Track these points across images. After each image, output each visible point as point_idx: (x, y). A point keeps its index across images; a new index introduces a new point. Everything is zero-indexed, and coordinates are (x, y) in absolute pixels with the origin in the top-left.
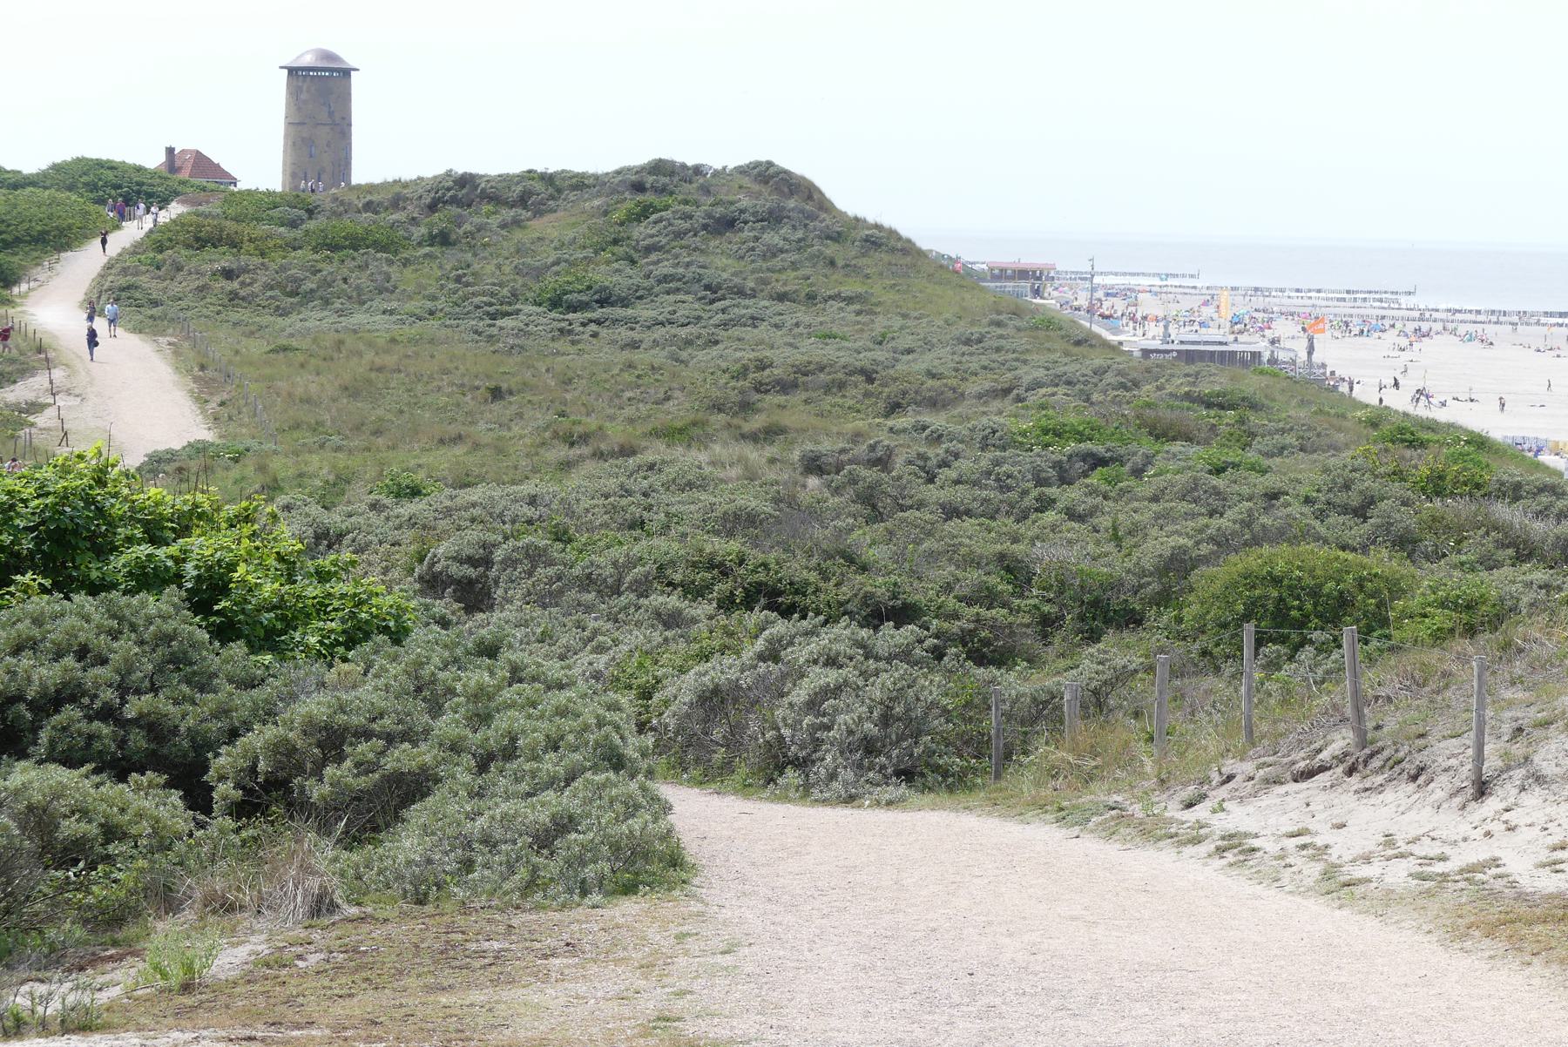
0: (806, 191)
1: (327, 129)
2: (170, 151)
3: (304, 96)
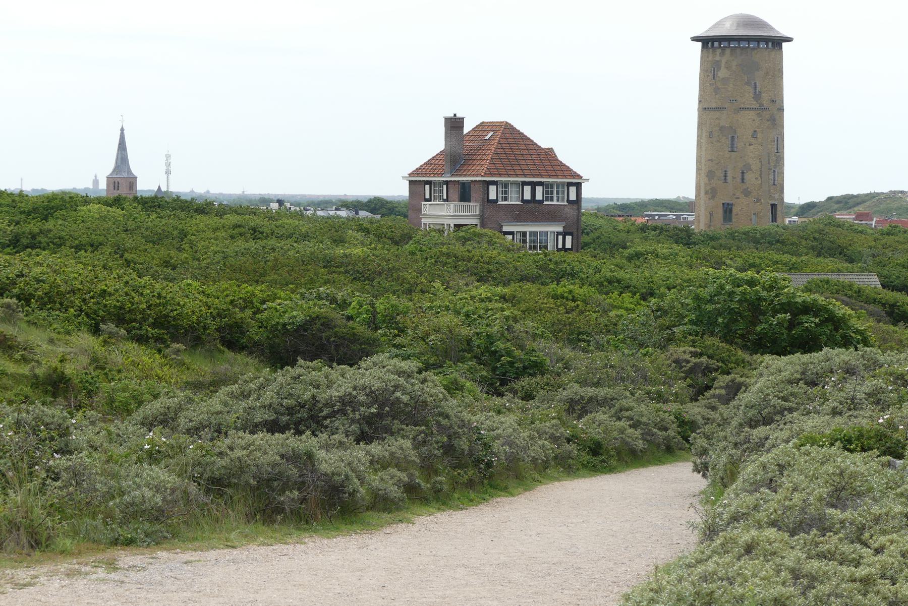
0: (544, 161)
1: (752, 114)
2: (454, 124)
3: (723, 73)
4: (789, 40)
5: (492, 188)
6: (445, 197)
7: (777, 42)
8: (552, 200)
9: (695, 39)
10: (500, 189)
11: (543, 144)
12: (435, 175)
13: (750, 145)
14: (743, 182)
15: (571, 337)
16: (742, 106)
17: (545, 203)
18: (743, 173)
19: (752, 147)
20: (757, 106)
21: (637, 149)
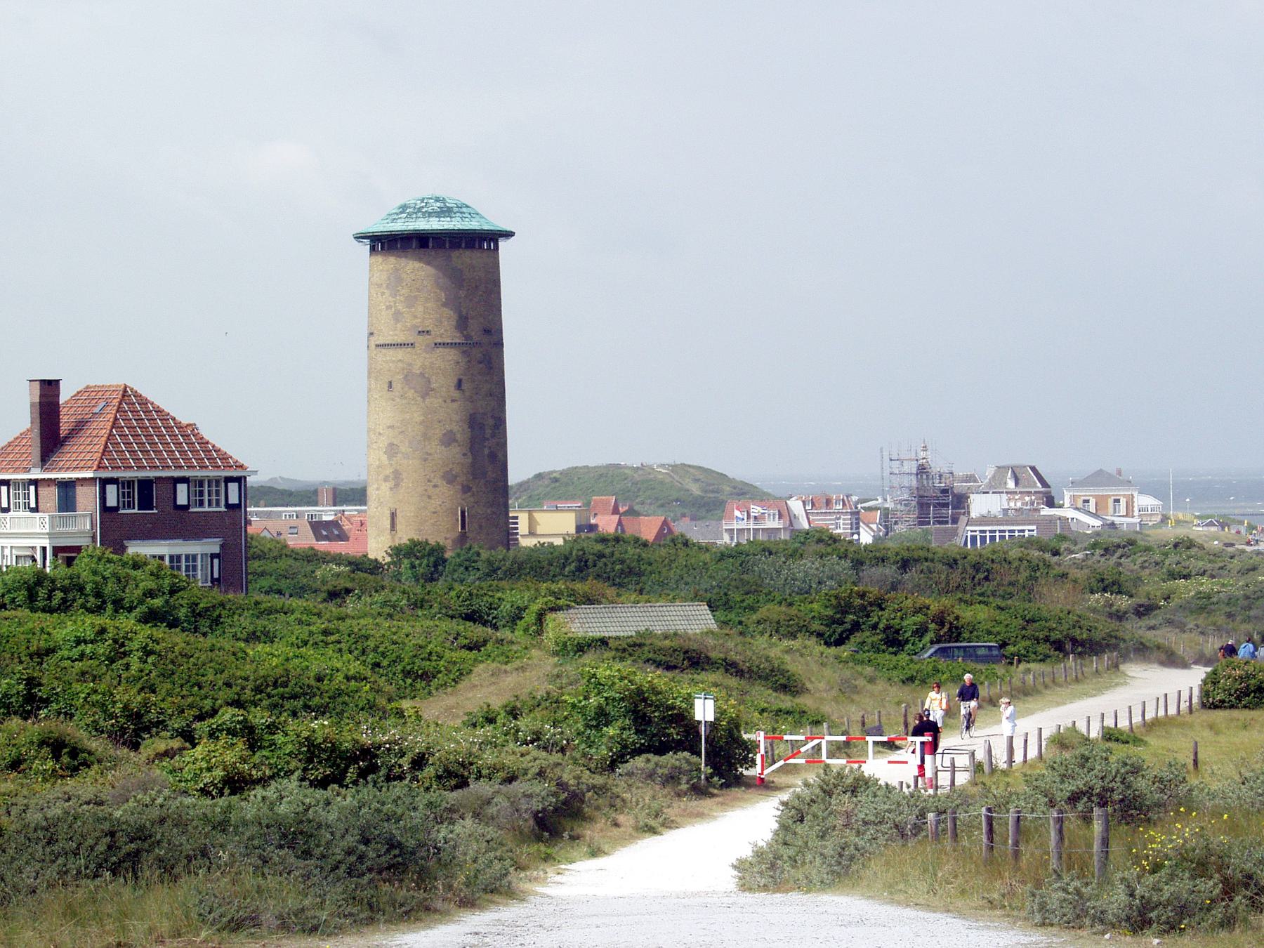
4: (508, 235)
5: (182, 489)
6: (33, 505)
8: (201, 504)
9: (360, 237)
10: (192, 489)
11: (183, 417)
12: (16, 470)
17: (121, 511)
21: (313, 419)
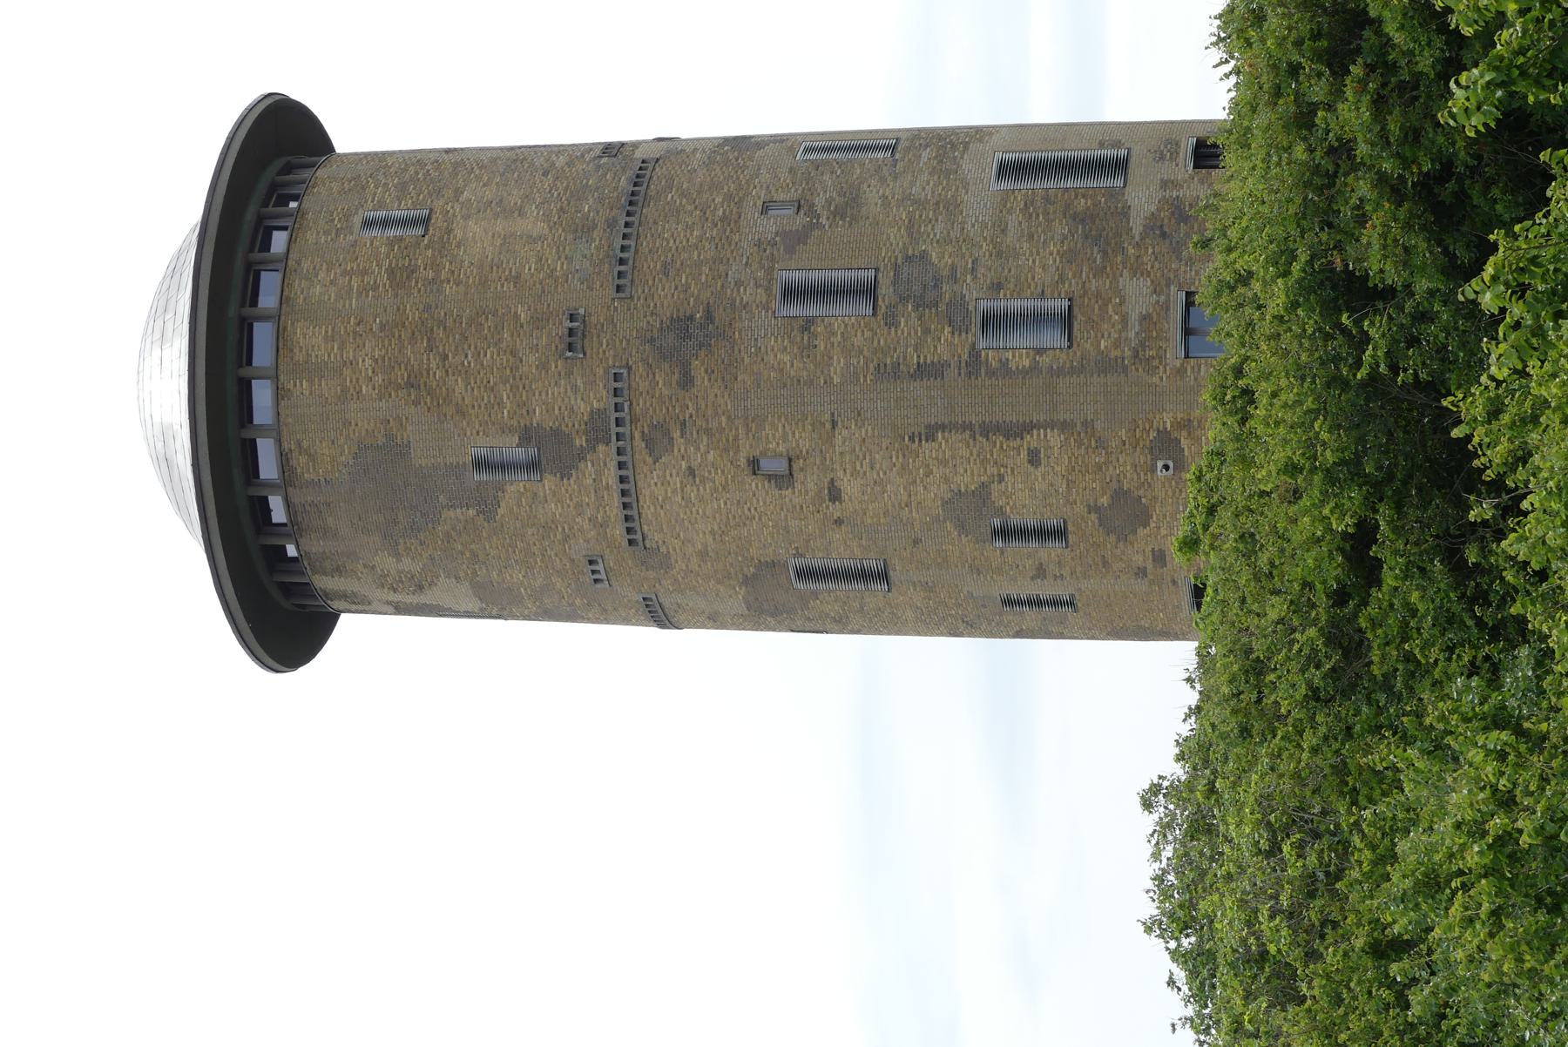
7: (275, 149)
13: (835, 495)
14: (1059, 533)
15: (1263, 560)
16: (618, 531)
18: (1005, 533)
19: (849, 487)
20: (606, 454)
